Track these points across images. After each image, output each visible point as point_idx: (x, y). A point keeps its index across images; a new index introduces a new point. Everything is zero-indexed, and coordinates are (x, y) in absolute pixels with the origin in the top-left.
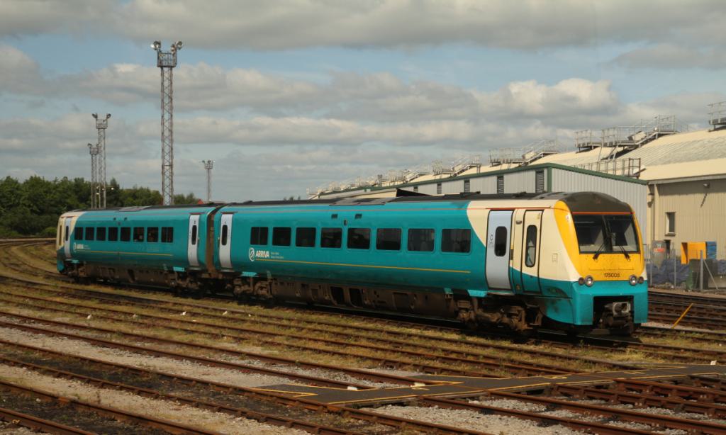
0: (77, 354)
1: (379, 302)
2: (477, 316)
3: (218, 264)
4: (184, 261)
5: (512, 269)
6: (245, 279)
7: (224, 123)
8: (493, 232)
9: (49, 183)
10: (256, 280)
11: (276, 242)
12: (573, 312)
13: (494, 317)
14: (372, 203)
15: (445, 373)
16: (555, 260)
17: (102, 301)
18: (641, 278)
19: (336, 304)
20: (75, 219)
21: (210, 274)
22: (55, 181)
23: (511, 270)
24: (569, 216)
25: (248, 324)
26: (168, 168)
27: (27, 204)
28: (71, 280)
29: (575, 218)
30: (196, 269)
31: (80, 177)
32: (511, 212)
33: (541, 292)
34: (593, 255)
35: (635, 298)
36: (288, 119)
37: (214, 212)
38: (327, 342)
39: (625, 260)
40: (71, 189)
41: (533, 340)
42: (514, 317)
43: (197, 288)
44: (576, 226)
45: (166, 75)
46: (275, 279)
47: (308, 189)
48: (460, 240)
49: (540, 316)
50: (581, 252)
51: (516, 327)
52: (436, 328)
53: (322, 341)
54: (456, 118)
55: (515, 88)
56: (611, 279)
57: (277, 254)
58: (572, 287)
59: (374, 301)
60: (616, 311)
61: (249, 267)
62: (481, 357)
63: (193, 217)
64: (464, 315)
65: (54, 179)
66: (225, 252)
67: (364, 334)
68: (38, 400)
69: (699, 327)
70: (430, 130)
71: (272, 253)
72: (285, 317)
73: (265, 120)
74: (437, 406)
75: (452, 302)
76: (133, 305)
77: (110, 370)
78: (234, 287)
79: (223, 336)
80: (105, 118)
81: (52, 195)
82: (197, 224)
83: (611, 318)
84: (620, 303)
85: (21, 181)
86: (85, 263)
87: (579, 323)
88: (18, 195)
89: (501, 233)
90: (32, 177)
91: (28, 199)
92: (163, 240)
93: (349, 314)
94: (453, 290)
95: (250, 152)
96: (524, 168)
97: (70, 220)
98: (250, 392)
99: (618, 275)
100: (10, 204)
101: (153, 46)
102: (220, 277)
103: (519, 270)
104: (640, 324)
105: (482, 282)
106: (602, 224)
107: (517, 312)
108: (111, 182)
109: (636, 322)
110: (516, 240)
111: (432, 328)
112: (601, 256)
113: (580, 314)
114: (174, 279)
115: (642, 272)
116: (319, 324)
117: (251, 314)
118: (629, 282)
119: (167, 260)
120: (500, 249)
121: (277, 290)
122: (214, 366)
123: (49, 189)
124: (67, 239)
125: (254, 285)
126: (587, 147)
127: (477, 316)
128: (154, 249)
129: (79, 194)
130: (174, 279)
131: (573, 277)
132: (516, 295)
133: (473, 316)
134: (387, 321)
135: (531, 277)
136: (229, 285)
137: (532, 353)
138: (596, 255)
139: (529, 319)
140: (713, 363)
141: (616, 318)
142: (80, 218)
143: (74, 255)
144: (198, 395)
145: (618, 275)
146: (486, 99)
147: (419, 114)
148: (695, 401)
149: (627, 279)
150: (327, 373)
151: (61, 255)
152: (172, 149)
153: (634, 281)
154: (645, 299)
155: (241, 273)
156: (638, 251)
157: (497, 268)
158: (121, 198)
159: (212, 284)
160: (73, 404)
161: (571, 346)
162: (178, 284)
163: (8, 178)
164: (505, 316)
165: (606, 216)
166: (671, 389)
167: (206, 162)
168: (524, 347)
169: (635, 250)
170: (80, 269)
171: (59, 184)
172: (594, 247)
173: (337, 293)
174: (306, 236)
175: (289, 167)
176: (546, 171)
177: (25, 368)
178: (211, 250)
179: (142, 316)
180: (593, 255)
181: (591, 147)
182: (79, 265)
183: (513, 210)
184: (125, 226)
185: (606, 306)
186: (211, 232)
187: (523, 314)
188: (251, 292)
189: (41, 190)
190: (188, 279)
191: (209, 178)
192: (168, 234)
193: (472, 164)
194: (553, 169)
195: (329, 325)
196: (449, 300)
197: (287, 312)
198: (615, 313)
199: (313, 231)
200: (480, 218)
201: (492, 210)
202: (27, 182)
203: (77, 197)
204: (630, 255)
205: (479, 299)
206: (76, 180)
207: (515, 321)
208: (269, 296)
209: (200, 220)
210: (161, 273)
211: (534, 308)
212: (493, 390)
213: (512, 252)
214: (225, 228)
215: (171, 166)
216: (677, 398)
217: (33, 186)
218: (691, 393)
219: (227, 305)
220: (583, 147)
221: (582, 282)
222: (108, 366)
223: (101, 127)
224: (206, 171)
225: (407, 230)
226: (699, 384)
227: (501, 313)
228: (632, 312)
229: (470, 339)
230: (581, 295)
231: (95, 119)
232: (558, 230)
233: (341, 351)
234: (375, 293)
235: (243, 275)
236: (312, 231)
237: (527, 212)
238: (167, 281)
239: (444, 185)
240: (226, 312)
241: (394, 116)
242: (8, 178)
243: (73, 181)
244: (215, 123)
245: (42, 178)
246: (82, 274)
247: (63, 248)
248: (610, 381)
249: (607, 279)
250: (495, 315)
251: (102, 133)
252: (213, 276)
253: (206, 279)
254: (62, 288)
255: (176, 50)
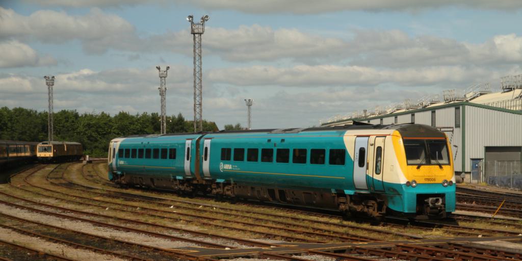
0: (79, 231)
1: (296, 199)
2: (350, 207)
3: (202, 174)
4: (182, 172)
5: (368, 176)
6: (218, 184)
7: (272, 70)
8: (357, 151)
9: (133, 117)
10: (225, 184)
11: (236, 159)
12: (403, 204)
13: (359, 208)
14: (293, 131)
15: (297, 241)
16: (392, 170)
17: (126, 200)
18: (451, 182)
19: (271, 200)
20: (119, 143)
21: (198, 181)
22: (138, 115)
23: (367, 177)
24: (401, 140)
25: (208, 213)
26: (198, 106)
27: (117, 132)
28: (118, 186)
29: (405, 142)
30: (189, 177)
31: (156, 112)
32: (384, 138)
33: (384, 191)
34: (416, 166)
35: (446, 196)
36: (321, 67)
37: (200, 138)
38: (244, 224)
39: (440, 169)
40: (149, 121)
41: (382, 223)
42: (370, 208)
43: (191, 190)
44: (406, 147)
45: (197, 40)
46: (236, 184)
47: (320, 121)
48: (339, 156)
49: (385, 207)
50: (408, 164)
51: (371, 215)
52: (328, 216)
53: (242, 223)
54: (453, 64)
55: (498, 40)
56: (429, 182)
57: (236, 166)
58: (402, 188)
59: (293, 198)
60: (432, 204)
61: (221, 175)
62: (332, 232)
63: (189, 142)
64: (342, 207)
65: (137, 114)
66: (206, 166)
67: (270, 218)
68: (28, 254)
69: (514, 217)
70: (431, 74)
71: (233, 166)
72: (234, 209)
73: (302, 67)
74: (268, 258)
75: (336, 198)
76: (143, 201)
77: (92, 239)
78: (212, 189)
79: (181, 220)
80: (165, 70)
81: (135, 126)
82: (190, 147)
83: (429, 208)
84: (435, 198)
85: (112, 116)
86: (125, 174)
87: (406, 211)
88: (110, 125)
89: (362, 152)
90: (120, 113)
91: (117, 129)
92: (249, 160)
93: (278, 207)
94: (336, 190)
95: (292, 92)
96: (425, 109)
97: (117, 143)
98: (162, 250)
99: (434, 180)
100: (104, 132)
101: (188, 19)
102: (204, 183)
103: (372, 176)
104: (451, 212)
105: (352, 185)
106: (424, 146)
107: (372, 205)
108: (178, 116)
109: (447, 211)
110: (370, 157)
111: (326, 216)
112: (422, 167)
113: (407, 205)
114: (176, 185)
115: (451, 178)
116: (254, 213)
117: (216, 208)
118: (443, 184)
119: (170, 171)
120: (362, 163)
121: (237, 191)
122: (174, 241)
123: (133, 121)
124: (114, 157)
125: (223, 188)
126: (509, 88)
127: (350, 207)
128: (325, 172)
129: (126, 125)
130: (176, 185)
131: (403, 181)
132: (371, 193)
133: (347, 208)
134: (301, 211)
135: (379, 181)
136: (209, 189)
137: (379, 232)
138: (419, 166)
139: (380, 209)
140: (480, 236)
141: (432, 208)
142: (122, 142)
143: (119, 169)
144: (130, 252)
145: (434, 180)
146: (475, 49)
147: (421, 62)
148: (406, 252)
149: (441, 182)
150: (7, 198)
151: (110, 169)
152: (201, 93)
153: (446, 184)
154: (454, 197)
155: (216, 180)
156: (449, 164)
157: (360, 175)
158: (185, 128)
159: (198, 188)
160: (46, 256)
161: (403, 226)
162: (180, 188)
163: (103, 113)
164: (366, 207)
165: (427, 141)
166: (423, 250)
167: (247, 101)
168: (375, 228)
169: (447, 162)
170: (122, 178)
171: (140, 118)
172: (418, 161)
173: (271, 192)
174: (300, 156)
175: (322, 103)
176: (461, 107)
177: (39, 238)
178: (198, 164)
179: (143, 208)
180: (416, 166)
181: (511, 88)
182: (122, 175)
183: (369, 136)
184: (148, 147)
185: (426, 200)
186: (198, 153)
187: (376, 206)
188: (222, 193)
189: (126, 122)
190: (185, 185)
191: (249, 112)
192: (171, 153)
193: (433, 101)
194: (466, 106)
195: (259, 214)
196: (334, 197)
197: (243, 206)
198: (431, 205)
199: (323, 151)
200: (351, 141)
201: (358, 136)
202: (116, 117)
203: (152, 127)
204: (443, 166)
205: (350, 196)
206: (152, 114)
207: (371, 210)
208: (233, 196)
209: (191, 143)
210: (170, 180)
211: (381, 202)
212: (311, 250)
213: (368, 164)
214: (206, 148)
215: (200, 104)
216: (426, 255)
217: (121, 119)
218: (434, 252)
219: (208, 202)
220: (506, 89)
221: (408, 184)
222: (91, 237)
223: (163, 77)
224: (247, 107)
225: (310, 150)
226: (453, 248)
227: (364, 206)
228: (444, 203)
229: (345, 223)
230: (408, 193)
231: (158, 70)
232: (394, 148)
233: (253, 230)
234: (293, 192)
235: (217, 181)
236: (304, 151)
237: (377, 138)
238: (173, 186)
239: (399, 117)
240: (201, 206)
241: (403, 63)
242: (103, 113)
243: (151, 115)
244: (266, 70)
245: (127, 113)
246: (123, 182)
247: (111, 164)
248: (393, 245)
249: (427, 182)
250: (360, 206)
251: (163, 81)
252: (200, 183)
253: (196, 184)
254: (107, 191)
255: (204, 22)
